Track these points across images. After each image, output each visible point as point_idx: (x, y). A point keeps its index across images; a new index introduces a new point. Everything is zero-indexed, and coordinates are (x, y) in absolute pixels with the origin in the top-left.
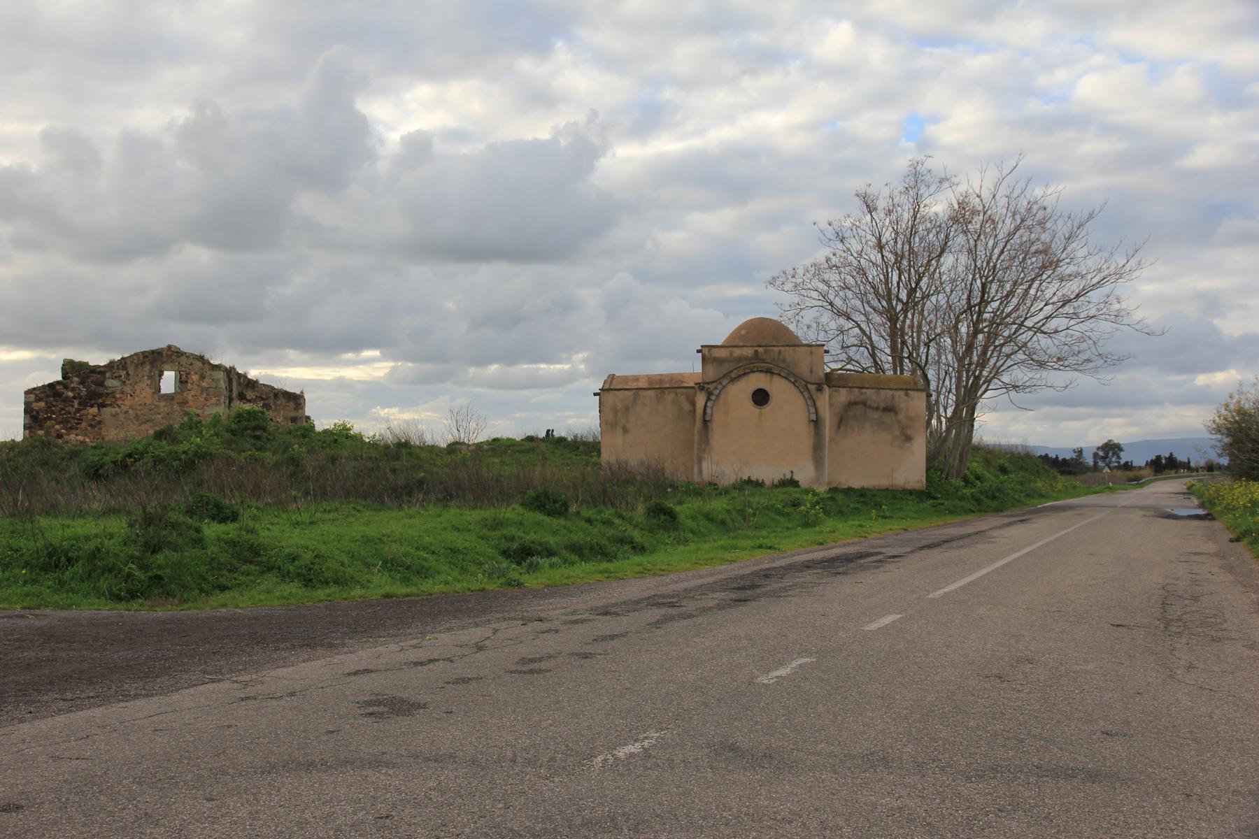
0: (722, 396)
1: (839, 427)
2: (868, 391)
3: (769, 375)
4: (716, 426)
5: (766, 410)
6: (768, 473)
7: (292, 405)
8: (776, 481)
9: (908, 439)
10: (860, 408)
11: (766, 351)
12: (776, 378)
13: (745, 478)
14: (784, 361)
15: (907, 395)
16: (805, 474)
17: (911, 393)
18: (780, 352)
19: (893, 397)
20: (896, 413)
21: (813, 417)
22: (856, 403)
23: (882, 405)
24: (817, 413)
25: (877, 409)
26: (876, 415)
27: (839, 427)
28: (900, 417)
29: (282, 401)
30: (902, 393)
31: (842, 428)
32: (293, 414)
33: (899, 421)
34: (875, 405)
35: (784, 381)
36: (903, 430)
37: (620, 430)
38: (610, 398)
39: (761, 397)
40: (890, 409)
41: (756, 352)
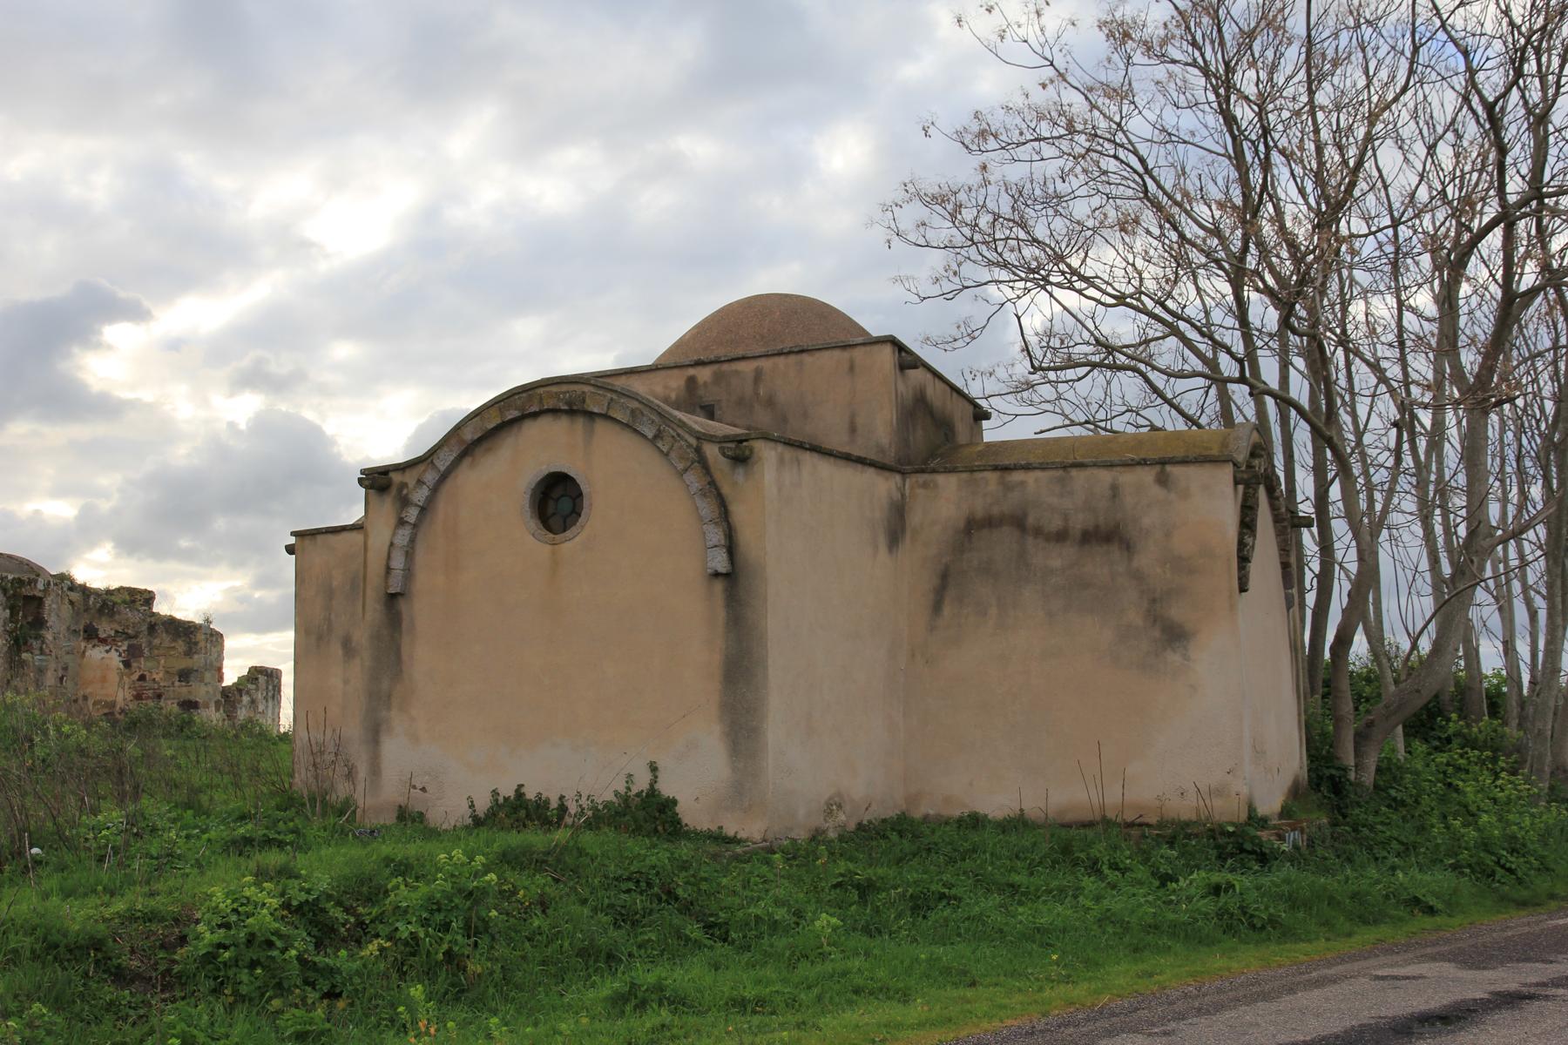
0: (442, 505)
1: (937, 607)
2: (1030, 478)
3: (580, 422)
4: (422, 611)
5: (573, 544)
6: (578, 770)
7: (181, 645)
8: (483, 804)
9: (1175, 636)
10: (1007, 534)
11: (718, 378)
12: (601, 427)
13: (508, 791)
14: (770, 402)
15: (1163, 480)
16: (696, 782)
17: (1175, 471)
18: (758, 376)
19: (1115, 490)
20: (1128, 547)
21: (720, 562)
22: (990, 522)
23: (1079, 522)
24: (731, 548)
25: (1061, 536)
26: (1056, 558)
27: (937, 607)
28: (1146, 559)
29: (163, 639)
30: (1147, 475)
31: (947, 610)
32: (184, 663)
33: (1138, 576)
34: (1055, 524)
35: (626, 440)
36: (1155, 606)
37: (336, 650)
38: (318, 554)
39: (557, 501)
40: (1107, 535)
41: (691, 381)
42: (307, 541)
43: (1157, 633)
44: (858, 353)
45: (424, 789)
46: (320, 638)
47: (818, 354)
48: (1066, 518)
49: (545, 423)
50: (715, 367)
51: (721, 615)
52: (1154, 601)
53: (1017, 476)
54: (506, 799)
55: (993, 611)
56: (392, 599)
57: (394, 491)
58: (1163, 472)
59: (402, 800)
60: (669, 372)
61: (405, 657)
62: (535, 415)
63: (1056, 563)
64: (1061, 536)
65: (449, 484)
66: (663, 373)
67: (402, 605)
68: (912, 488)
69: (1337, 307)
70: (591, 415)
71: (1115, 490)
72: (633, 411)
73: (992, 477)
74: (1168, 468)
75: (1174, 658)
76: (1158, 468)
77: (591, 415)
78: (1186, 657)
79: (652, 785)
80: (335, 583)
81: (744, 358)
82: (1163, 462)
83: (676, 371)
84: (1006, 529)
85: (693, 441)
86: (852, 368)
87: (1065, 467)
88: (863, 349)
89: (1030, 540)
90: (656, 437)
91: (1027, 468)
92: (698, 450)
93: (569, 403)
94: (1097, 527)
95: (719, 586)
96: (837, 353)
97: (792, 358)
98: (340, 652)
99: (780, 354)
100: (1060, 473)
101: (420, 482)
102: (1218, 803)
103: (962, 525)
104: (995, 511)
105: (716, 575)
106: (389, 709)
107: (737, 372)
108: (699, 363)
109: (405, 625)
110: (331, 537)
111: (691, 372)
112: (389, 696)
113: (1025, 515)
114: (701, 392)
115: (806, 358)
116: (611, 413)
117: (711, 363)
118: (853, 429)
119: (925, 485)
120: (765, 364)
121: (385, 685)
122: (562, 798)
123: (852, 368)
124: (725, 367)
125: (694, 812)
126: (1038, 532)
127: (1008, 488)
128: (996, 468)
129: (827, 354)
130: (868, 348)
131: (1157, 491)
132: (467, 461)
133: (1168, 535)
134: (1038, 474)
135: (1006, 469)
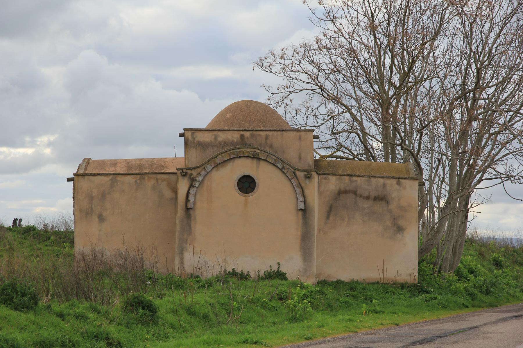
0: (206, 182)
1: (328, 217)
2: (359, 179)
3: (255, 161)
4: (199, 214)
5: (252, 197)
6: (254, 265)
8: (262, 274)
10: (351, 196)
11: (252, 136)
12: (262, 162)
13: (230, 270)
14: (271, 146)
15: (398, 183)
16: (292, 266)
18: (267, 137)
19: (384, 185)
20: (388, 202)
22: (346, 192)
23: (373, 194)
25: (368, 198)
26: (366, 204)
27: (328, 217)
28: (393, 206)
30: (394, 182)
31: (331, 218)
33: (390, 211)
34: (366, 194)
35: (271, 168)
37: (95, 219)
38: (84, 183)
39: (247, 184)
40: (381, 199)
41: (242, 136)
42: (80, 178)
43: (395, 229)
44: (302, 134)
45: (199, 269)
46: (87, 213)
47: (288, 132)
48: (369, 192)
49: (243, 160)
50: (251, 132)
51: (301, 221)
52: (394, 219)
53: (354, 178)
54: (229, 272)
55: (346, 219)
56: (187, 209)
57: (188, 176)
58: (399, 181)
59: (192, 272)
60: (234, 132)
61: (192, 228)
62: (240, 157)
63: (366, 206)
64: (368, 198)
65: (209, 175)
66: (231, 132)
67: (191, 212)
68: (321, 179)
69: (362, 81)
70: (259, 159)
71: (384, 185)
72: (275, 160)
73: (347, 178)
74: (400, 180)
75: (399, 236)
76: (397, 180)
77: (259, 159)
78: (403, 236)
79: (278, 269)
80: (94, 194)
81: (262, 130)
82: (399, 178)
83: (236, 132)
84: (351, 194)
85: (293, 170)
86: (300, 138)
87: (370, 177)
88: (304, 132)
89: (358, 198)
90: (282, 168)
91: (358, 176)
92: (294, 173)
93: (254, 155)
94: (379, 196)
95: (300, 213)
96: (295, 133)
97: (279, 133)
98: (97, 219)
99: (275, 130)
100: (368, 178)
101: (199, 174)
102: (399, 278)
103: (337, 192)
104: (348, 188)
105: (301, 210)
106: (187, 244)
107: (259, 135)
108: (246, 130)
109: (192, 218)
110: (92, 178)
111: (242, 133)
112: (187, 240)
113: (357, 191)
114: (246, 140)
115: (284, 132)
116: (268, 160)
117: (250, 131)
118: (300, 158)
119: (325, 179)
120: (270, 133)
121: (185, 236)
122: (248, 272)
123: (300, 138)
124: (255, 133)
125: (291, 276)
126: (361, 196)
127: (352, 182)
128: (348, 175)
129: (291, 132)
130: (306, 132)
131: (397, 187)
132: (216, 168)
133: (399, 200)
134: (361, 178)
135: (351, 176)
